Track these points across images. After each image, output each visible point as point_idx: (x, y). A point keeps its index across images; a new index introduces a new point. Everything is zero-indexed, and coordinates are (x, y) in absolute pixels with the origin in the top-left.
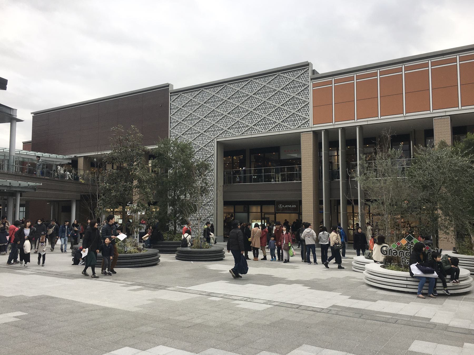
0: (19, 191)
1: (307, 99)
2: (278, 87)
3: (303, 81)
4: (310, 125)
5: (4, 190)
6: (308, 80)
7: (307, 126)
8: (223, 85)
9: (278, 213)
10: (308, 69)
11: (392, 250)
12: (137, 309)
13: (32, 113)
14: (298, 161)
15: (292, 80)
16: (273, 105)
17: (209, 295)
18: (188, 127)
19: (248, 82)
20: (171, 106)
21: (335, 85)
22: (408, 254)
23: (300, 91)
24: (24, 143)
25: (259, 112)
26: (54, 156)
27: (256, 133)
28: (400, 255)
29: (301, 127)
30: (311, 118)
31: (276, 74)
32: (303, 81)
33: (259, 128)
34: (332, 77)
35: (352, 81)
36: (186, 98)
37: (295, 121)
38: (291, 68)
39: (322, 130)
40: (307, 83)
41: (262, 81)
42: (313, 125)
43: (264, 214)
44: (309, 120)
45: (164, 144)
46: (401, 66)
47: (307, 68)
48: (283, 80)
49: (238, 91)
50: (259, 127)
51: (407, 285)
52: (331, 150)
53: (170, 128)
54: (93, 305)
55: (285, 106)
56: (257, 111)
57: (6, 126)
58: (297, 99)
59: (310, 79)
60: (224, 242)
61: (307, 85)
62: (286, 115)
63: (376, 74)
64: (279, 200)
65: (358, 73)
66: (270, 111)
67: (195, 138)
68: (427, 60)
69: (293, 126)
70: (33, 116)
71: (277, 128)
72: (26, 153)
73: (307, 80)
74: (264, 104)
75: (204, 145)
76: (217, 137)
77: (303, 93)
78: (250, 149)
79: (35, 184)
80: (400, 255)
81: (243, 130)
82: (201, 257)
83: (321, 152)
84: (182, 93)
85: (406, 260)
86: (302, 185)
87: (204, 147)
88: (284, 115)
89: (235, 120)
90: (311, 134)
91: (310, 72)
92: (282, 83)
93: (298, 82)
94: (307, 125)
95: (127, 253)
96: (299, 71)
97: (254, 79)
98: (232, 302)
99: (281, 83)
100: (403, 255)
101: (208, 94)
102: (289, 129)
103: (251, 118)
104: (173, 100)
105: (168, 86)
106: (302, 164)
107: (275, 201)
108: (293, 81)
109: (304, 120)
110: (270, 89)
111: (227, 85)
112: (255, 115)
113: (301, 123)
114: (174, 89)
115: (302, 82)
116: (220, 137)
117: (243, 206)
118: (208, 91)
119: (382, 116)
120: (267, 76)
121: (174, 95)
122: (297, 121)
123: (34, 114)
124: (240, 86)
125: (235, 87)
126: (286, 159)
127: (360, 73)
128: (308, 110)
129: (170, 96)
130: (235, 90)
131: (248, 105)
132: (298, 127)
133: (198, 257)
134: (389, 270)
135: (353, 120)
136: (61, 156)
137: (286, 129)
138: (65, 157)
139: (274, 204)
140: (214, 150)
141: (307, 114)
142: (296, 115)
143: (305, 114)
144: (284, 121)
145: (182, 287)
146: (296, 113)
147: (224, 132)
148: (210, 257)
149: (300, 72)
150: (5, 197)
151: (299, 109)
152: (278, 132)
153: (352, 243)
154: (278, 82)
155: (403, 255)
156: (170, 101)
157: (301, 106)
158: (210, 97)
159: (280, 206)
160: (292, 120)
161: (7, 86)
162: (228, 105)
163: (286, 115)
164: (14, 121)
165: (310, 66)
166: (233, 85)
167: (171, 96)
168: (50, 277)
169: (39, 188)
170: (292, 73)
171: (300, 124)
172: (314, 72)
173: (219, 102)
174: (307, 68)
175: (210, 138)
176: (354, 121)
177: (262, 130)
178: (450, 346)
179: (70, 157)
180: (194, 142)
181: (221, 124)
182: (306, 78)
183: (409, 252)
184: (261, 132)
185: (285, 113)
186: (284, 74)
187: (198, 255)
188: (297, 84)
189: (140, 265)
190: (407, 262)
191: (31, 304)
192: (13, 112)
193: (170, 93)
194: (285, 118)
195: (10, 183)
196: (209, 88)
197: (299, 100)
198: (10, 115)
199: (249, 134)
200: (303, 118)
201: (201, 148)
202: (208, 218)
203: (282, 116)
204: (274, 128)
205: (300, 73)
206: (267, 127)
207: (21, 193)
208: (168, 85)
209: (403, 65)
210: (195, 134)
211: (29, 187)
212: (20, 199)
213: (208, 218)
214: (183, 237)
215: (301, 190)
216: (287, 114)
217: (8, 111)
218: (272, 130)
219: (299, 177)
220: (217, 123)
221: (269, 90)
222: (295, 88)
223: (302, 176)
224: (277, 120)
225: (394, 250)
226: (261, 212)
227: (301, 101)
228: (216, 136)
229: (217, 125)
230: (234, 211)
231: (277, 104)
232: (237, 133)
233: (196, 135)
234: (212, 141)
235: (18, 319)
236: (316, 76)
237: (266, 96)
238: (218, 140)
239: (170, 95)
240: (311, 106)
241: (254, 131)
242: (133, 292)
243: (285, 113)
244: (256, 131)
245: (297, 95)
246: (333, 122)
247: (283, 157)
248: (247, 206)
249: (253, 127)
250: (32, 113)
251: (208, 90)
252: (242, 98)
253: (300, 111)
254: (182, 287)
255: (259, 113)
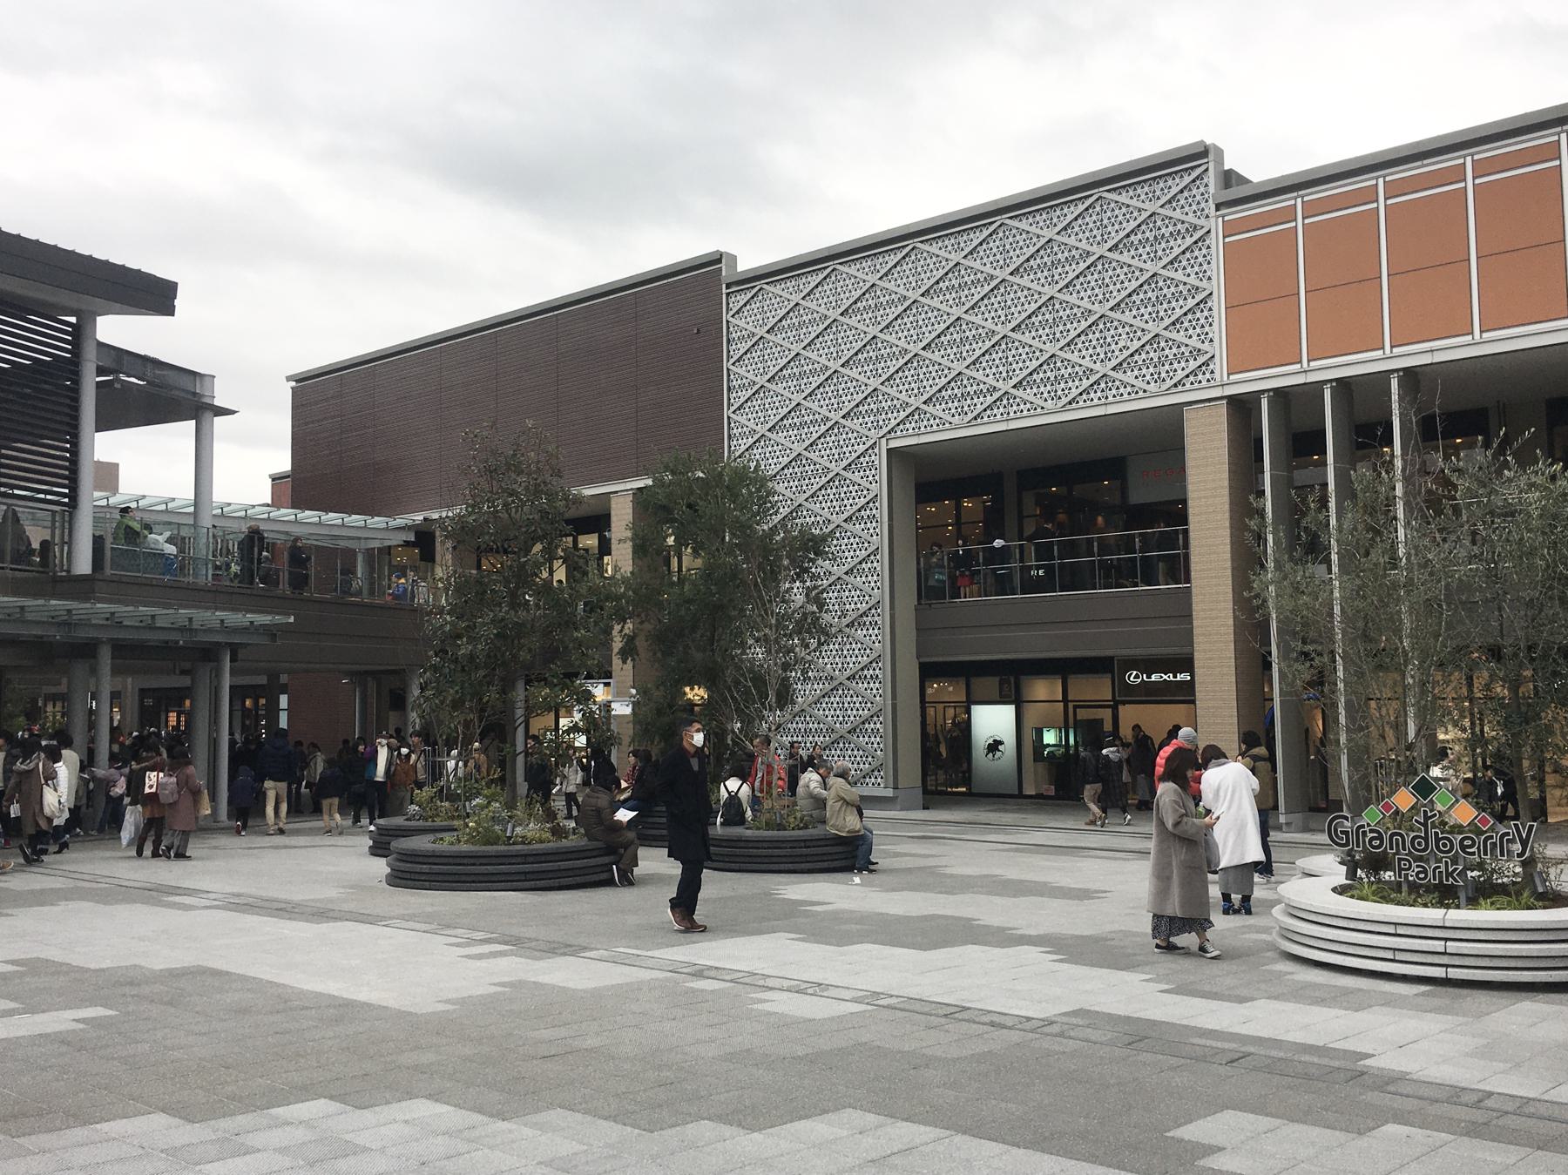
0: (226, 643)
1: (1205, 281)
2: (1099, 243)
3: (1187, 214)
4: (1217, 375)
5: (177, 642)
6: (1206, 211)
7: (1208, 381)
8: (904, 247)
9: (1124, 703)
10: (1207, 170)
11: (1367, 829)
12: (441, 1007)
13: (289, 379)
14: (1177, 513)
15: (1149, 213)
16: (1188, 287)
17: (699, 974)
18: (787, 402)
19: (905, 251)
20: (731, 329)
21: (1307, 221)
22: (1445, 845)
23: (1177, 251)
24: (273, 480)
25: (943, 357)
26: (356, 520)
27: (935, 427)
28: (1391, 848)
29: (1078, 402)
30: (1220, 349)
31: (1092, 195)
32: (1187, 214)
33: (1035, 395)
34: (1295, 194)
35: (1552, 160)
36: (934, 259)
37: (1163, 365)
38: (1159, 164)
39: (1263, 392)
40: (1202, 222)
41: (950, 248)
42: (1229, 374)
43: (1075, 707)
44: (1213, 357)
45: (673, 473)
46: (1556, 138)
47: (1200, 165)
48: (1018, 242)
49: (1048, 242)
50: (1035, 390)
51: (1395, 950)
52: (1296, 468)
53: (729, 409)
54: (319, 995)
55: (1023, 333)
56: (1027, 334)
57: (185, 430)
58: (1064, 305)
59: (1213, 207)
60: (926, 812)
61: (1205, 230)
62: (1129, 344)
63: (1370, 195)
64: (1153, 653)
65: (1392, 174)
66: (1177, 310)
67: (811, 440)
68: (1289, 199)
69: (1053, 399)
70: (292, 388)
71: (1099, 394)
72: (266, 516)
73: (1203, 210)
74: (1050, 308)
75: (845, 463)
76: (889, 432)
77: (986, 306)
78: (1018, 472)
79: (270, 618)
80: (1391, 848)
81: (1073, 390)
82: (774, 860)
83: (1260, 476)
84: (767, 283)
85: (1414, 865)
86: (1195, 599)
87: (843, 472)
88: (1120, 345)
89: (1041, 351)
90: (1223, 409)
91: (1211, 178)
92: (1113, 225)
93: (1171, 218)
94: (1208, 376)
95: (514, 844)
96: (1174, 179)
97: (1108, 191)
98: (691, 985)
99: (1110, 228)
100: (1404, 849)
101: (853, 280)
102: (1141, 393)
103: (1004, 361)
104: (735, 310)
105: (719, 261)
106: (1191, 519)
107: (1112, 658)
108: (1151, 216)
109: (1088, 378)
110: (976, 274)
111: (919, 245)
112: (1017, 349)
113: (1183, 369)
114: (740, 268)
115: (1183, 218)
116: (899, 433)
117: (997, 679)
118: (852, 270)
119: (1232, 374)
120: (964, 231)
121: (738, 291)
122: (1140, 369)
123: (297, 381)
124: (1158, 193)
125: (1039, 228)
126: (1160, 503)
127: (1437, 163)
128: (1210, 320)
129: (724, 296)
130: (947, 260)
131: (906, 333)
132: (1175, 386)
133: (766, 860)
134: (1354, 900)
135: (1468, 334)
136: (378, 521)
137: (1129, 394)
138: (393, 523)
139: (1112, 672)
140: (876, 481)
141: (1205, 337)
142: (1167, 341)
143: (994, 374)
144: (1121, 364)
145: (634, 951)
146: (1167, 334)
147: (1097, 382)
148: (804, 858)
149: (1072, 208)
150: (187, 665)
151: (1177, 320)
152: (1104, 407)
153: (725, 786)
154: (1098, 224)
155: (1404, 849)
156: (727, 313)
157: (1181, 307)
158: (1032, 250)
159: (1133, 677)
160: (1152, 359)
161: (176, 302)
162: (1012, 295)
163: (1129, 344)
164: (208, 415)
165: (1211, 157)
166: (858, 266)
167: (728, 294)
168: (256, 918)
169: (285, 629)
170: (1044, 216)
171: (1180, 374)
172: (1229, 178)
173: (893, 309)
174: (1200, 165)
175: (864, 439)
176: (1470, 337)
177: (953, 416)
178: (1329, 1131)
179: (410, 523)
180: (811, 455)
181: (822, 402)
182: (1091, 230)
183: (1421, 837)
184: (1043, 408)
185: (1124, 336)
186: (1120, 194)
187: (765, 852)
188: (1167, 227)
189: (555, 882)
190: (1416, 870)
191: (146, 990)
192: (202, 386)
193: (724, 286)
194: (1126, 353)
195: (222, 621)
196: (939, 237)
197: (1072, 308)
198: (195, 394)
199: (999, 417)
200: (1084, 372)
201: (834, 473)
202: (863, 723)
203: (1113, 346)
204: (1088, 393)
205: (1176, 185)
206: (1063, 390)
207: (234, 649)
208: (716, 259)
209: (1562, 132)
210: (811, 426)
211: (252, 630)
212: (231, 669)
213: (863, 723)
214: (724, 794)
215: (1191, 615)
216: (1132, 340)
217: (185, 382)
218: (985, 415)
219: (1179, 569)
220: (886, 383)
221: (972, 277)
222: (1056, 268)
223: (1193, 567)
224: (1098, 364)
225: (1371, 831)
226: (1065, 700)
227: (1075, 310)
228: (885, 430)
229: (889, 390)
230: (968, 694)
231: (1096, 305)
232: (957, 417)
233: (817, 428)
234: (872, 447)
235: (81, 1026)
236: (1236, 192)
237: (963, 299)
238: (893, 444)
239: (724, 291)
240: (1219, 304)
241: (1015, 408)
242: (470, 962)
243: (1124, 336)
244: (1022, 406)
245: (1064, 290)
246: (1300, 362)
247: (1137, 496)
248: (1012, 680)
249: (924, 407)
250: (289, 379)
251: (934, 245)
252: (973, 290)
253: (1178, 326)
254: (634, 951)
255: (940, 360)
